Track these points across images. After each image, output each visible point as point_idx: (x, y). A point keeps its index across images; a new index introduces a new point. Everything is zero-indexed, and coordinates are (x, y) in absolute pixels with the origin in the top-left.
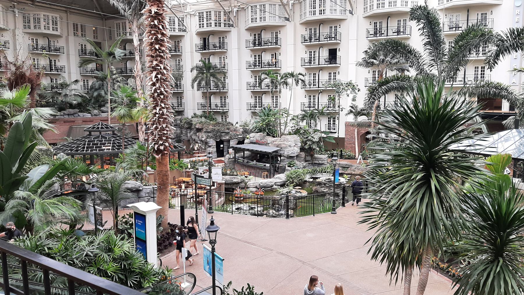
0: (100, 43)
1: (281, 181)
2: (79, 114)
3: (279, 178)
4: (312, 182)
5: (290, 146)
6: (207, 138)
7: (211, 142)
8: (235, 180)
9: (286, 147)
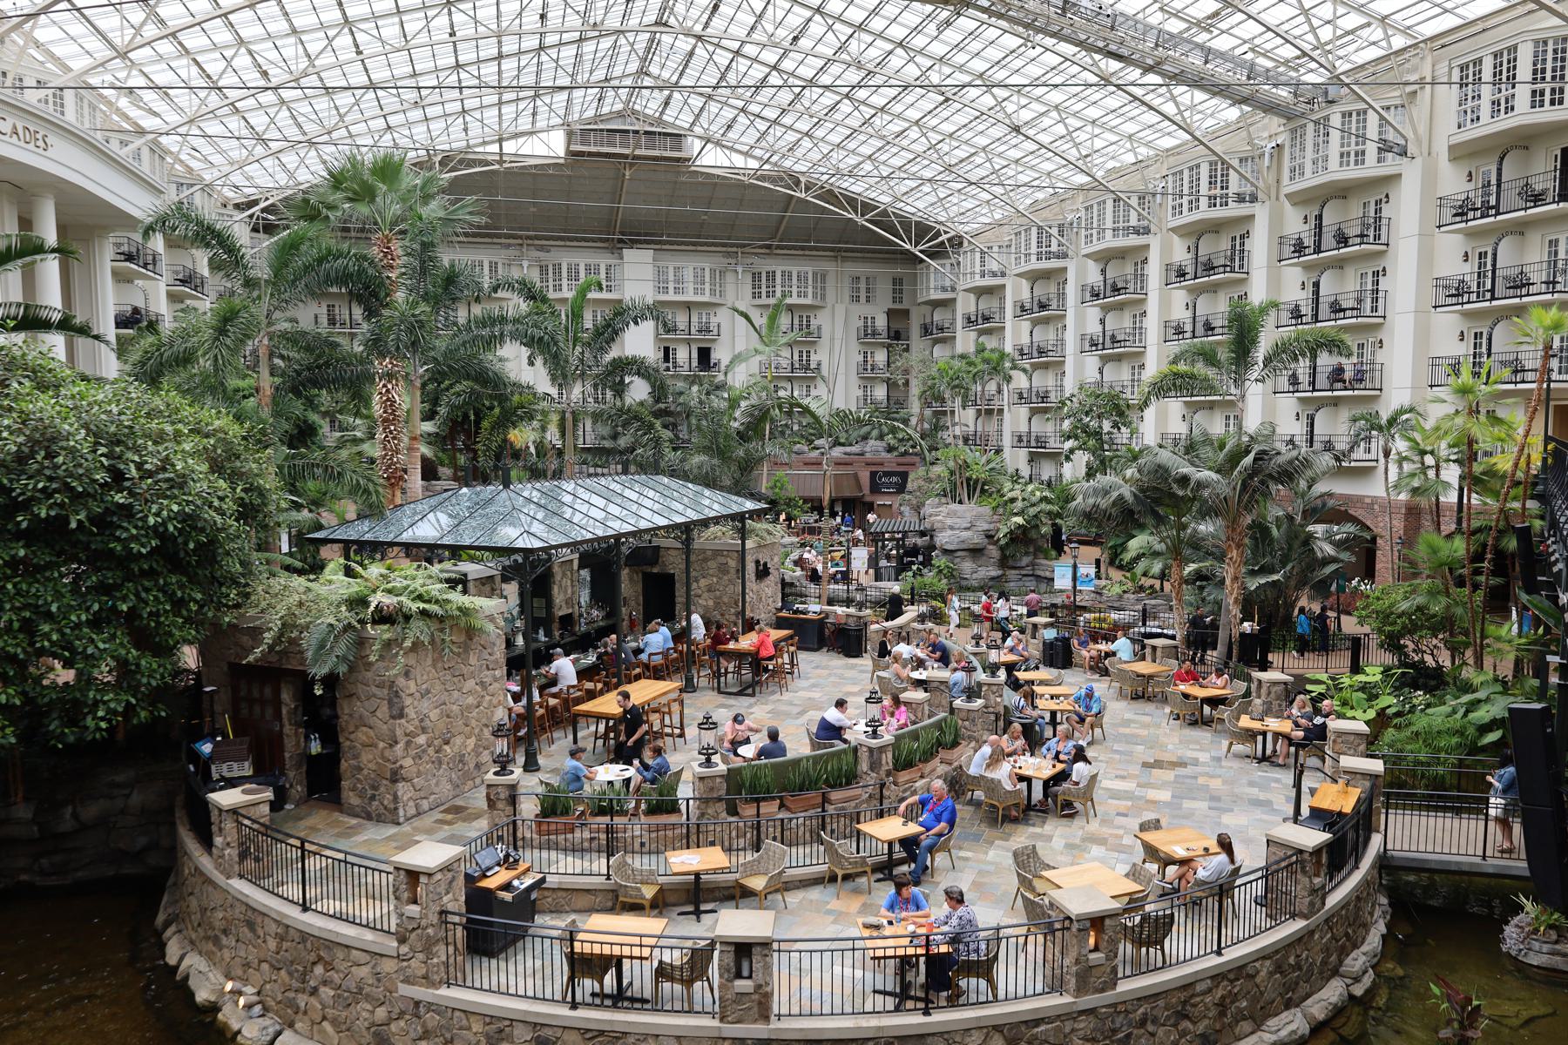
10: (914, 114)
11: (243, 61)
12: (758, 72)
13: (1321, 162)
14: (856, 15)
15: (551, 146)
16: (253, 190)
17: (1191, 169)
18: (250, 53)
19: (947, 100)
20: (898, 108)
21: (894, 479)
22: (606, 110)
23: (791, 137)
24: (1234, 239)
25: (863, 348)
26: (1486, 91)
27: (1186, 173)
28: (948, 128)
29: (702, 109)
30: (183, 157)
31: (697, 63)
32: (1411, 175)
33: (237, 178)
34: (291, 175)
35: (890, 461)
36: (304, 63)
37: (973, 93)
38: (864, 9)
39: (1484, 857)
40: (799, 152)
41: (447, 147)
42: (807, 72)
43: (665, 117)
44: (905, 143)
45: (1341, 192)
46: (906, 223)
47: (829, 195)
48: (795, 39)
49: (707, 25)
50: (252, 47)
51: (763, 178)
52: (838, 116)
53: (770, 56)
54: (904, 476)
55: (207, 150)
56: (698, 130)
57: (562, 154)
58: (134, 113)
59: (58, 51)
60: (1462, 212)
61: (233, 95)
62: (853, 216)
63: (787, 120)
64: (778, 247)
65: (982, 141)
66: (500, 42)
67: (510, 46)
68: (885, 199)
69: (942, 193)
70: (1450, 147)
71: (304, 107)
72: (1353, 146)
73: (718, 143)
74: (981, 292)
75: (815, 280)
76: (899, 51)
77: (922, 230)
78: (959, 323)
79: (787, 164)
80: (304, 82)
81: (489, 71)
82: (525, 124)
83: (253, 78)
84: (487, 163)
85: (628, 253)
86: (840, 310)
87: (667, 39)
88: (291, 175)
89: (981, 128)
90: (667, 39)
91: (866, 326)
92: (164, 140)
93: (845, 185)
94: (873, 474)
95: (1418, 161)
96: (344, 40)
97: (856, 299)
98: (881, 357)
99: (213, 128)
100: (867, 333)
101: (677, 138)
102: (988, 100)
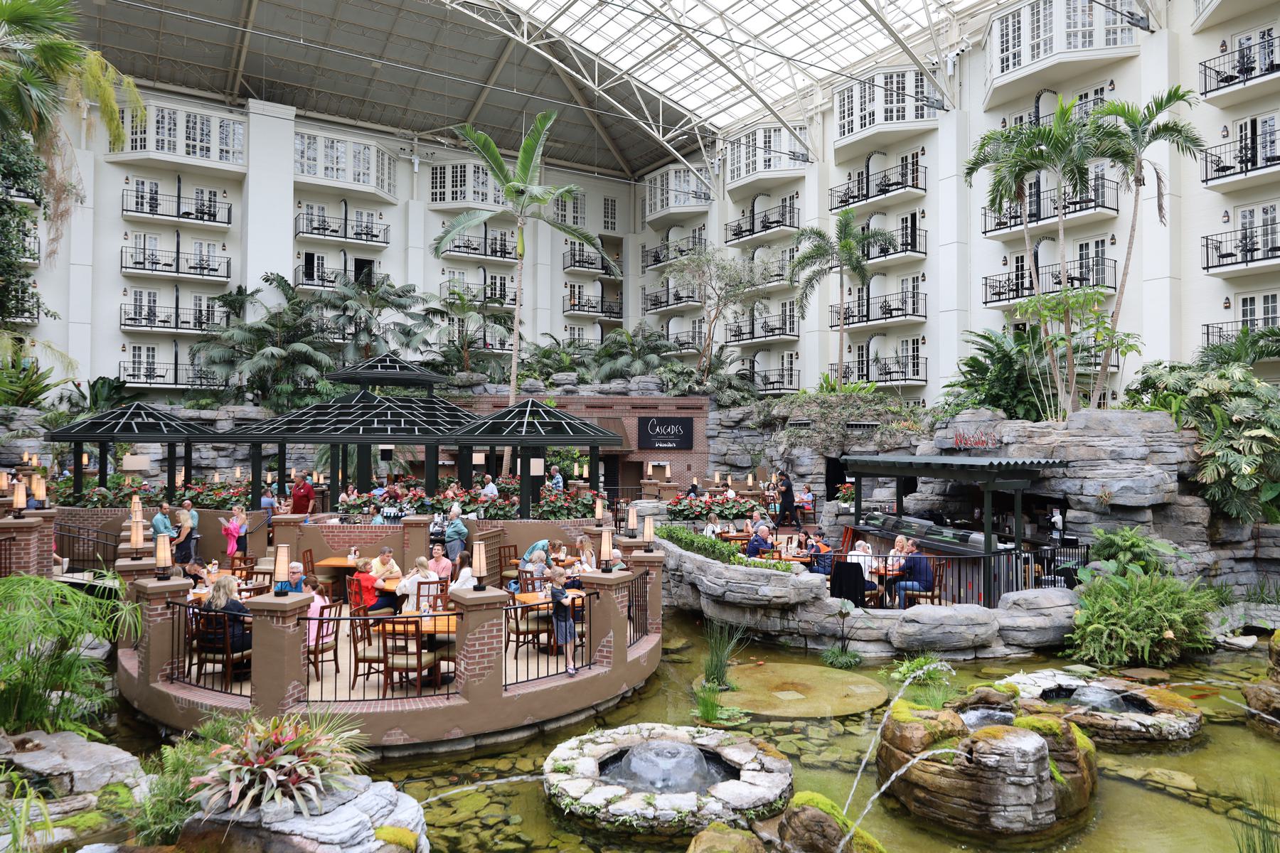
0: (621, 239)
1: (1040, 622)
2: (488, 386)
3: (1033, 609)
4: (1253, 649)
5: (1118, 457)
6: (793, 446)
7: (806, 461)
8: (769, 591)
9: (1094, 462)
13: (751, 166)
17: (747, 136)
21: (673, 429)
24: (694, 231)
25: (571, 281)
26: (760, 153)
27: (1010, 18)
32: (811, 174)
35: (667, 404)
39: (176, 383)
45: (881, 146)
54: (687, 424)
60: (738, 233)
62: (590, 83)
70: (837, 151)
72: (1080, 27)
94: (643, 422)
95: (953, 112)
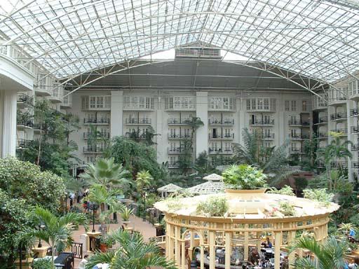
10: (306, 39)
11: (64, 33)
12: (246, 26)
14: (282, 4)
15: (169, 55)
16: (66, 76)
18: (66, 30)
19: (319, 34)
20: (300, 37)
22: (190, 42)
23: (260, 49)
28: (320, 44)
29: (226, 40)
30: (44, 65)
31: (223, 23)
33: (61, 71)
34: (78, 69)
36: (83, 32)
37: (328, 31)
38: (285, 2)
40: (263, 54)
41: (132, 57)
42: (264, 25)
43: (212, 43)
44: (304, 50)
46: (306, 80)
47: (276, 70)
48: (259, 14)
49: (226, 10)
50: (67, 28)
51: (249, 64)
52: (277, 41)
53: (251, 20)
55: (51, 63)
56: (224, 47)
57: (174, 58)
58: (29, 52)
59: (7, 34)
61: (60, 44)
63: (258, 42)
64: (257, 90)
65: (334, 48)
66: (151, 20)
67: (154, 21)
68: (298, 71)
69: (319, 68)
71: (83, 47)
73: (232, 52)
74: (337, 106)
75: (271, 102)
76: (299, 16)
77: (313, 82)
78: (329, 118)
79: (259, 58)
80: (83, 38)
81: (147, 31)
82: (160, 47)
83: (66, 38)
84: (146, 62)
85: (113, 93)
86: (242, 113)
87: (212, 16)
88: (78, 69)
89: (333, 43)
90: (212, 16)
91: (292, 119)
92: (38, 60)
93: (282, 66)
96: (97, 24)
97: (287, 109)
98: (298, 132)
99: (53, 55)
100: (292, 122)
101: (217, 51)
102: (334, 34)
